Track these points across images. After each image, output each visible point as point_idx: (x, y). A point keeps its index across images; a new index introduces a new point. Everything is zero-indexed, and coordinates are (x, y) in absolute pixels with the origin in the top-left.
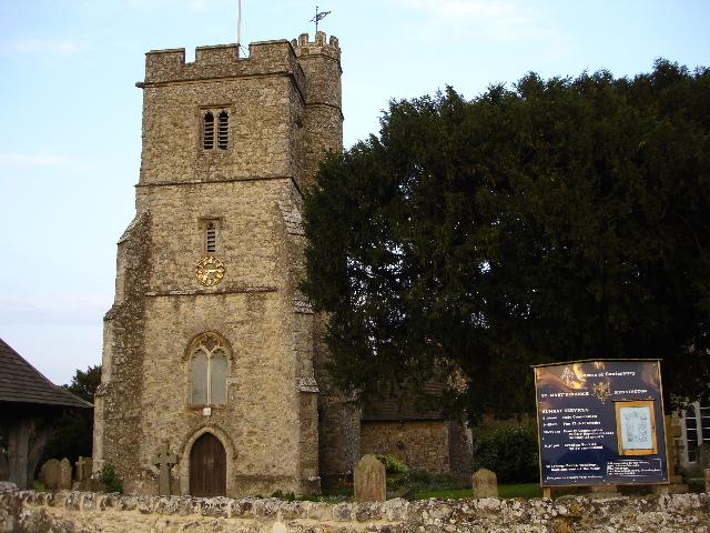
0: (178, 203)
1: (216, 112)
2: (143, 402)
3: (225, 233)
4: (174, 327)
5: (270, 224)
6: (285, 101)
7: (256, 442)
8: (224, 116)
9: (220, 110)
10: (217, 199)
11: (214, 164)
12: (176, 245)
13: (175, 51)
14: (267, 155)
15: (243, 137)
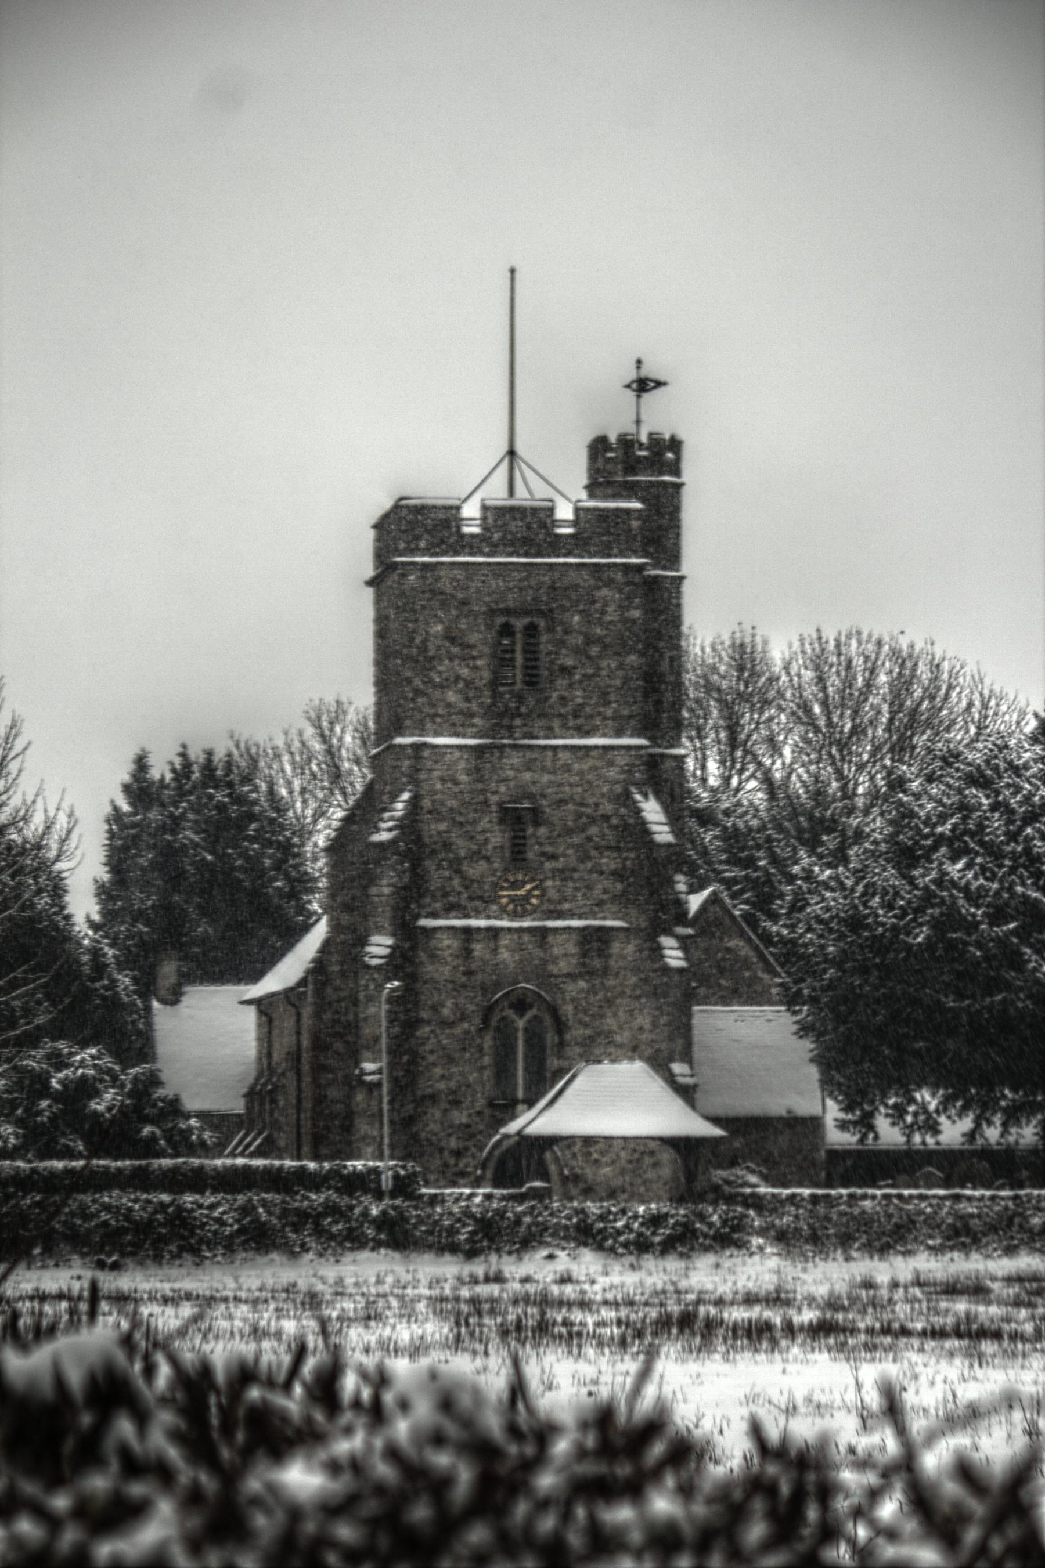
0: (463, 778)
1: (519, 624)
2: (419, 1093)
3: (543, 831)
4: (464, 979)
5: (614, 821)
6: (636, 614)
7: (595, 1156)
8: (531, 630)
9: (527, 620)
10: (527, 776)
11: (520, 715)
12: (462, 846)
13: (451, 508)
14: (608, 703)
15: (565, 671)
